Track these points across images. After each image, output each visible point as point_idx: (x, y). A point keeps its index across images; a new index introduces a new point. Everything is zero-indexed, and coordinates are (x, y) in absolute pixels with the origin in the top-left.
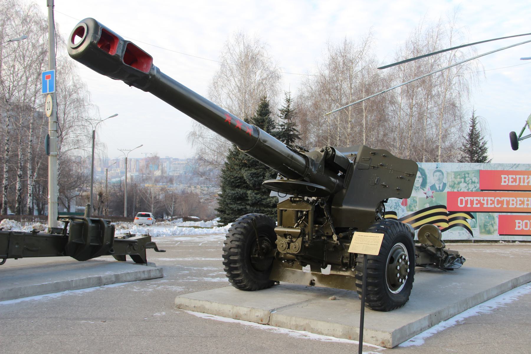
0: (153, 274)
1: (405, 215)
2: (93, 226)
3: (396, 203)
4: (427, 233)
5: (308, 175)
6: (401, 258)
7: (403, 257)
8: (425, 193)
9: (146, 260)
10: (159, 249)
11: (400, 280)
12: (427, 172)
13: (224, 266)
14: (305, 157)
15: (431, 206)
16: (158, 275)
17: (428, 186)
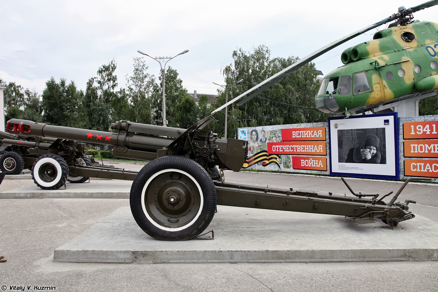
12: (258, 132)
17: (259, 140)
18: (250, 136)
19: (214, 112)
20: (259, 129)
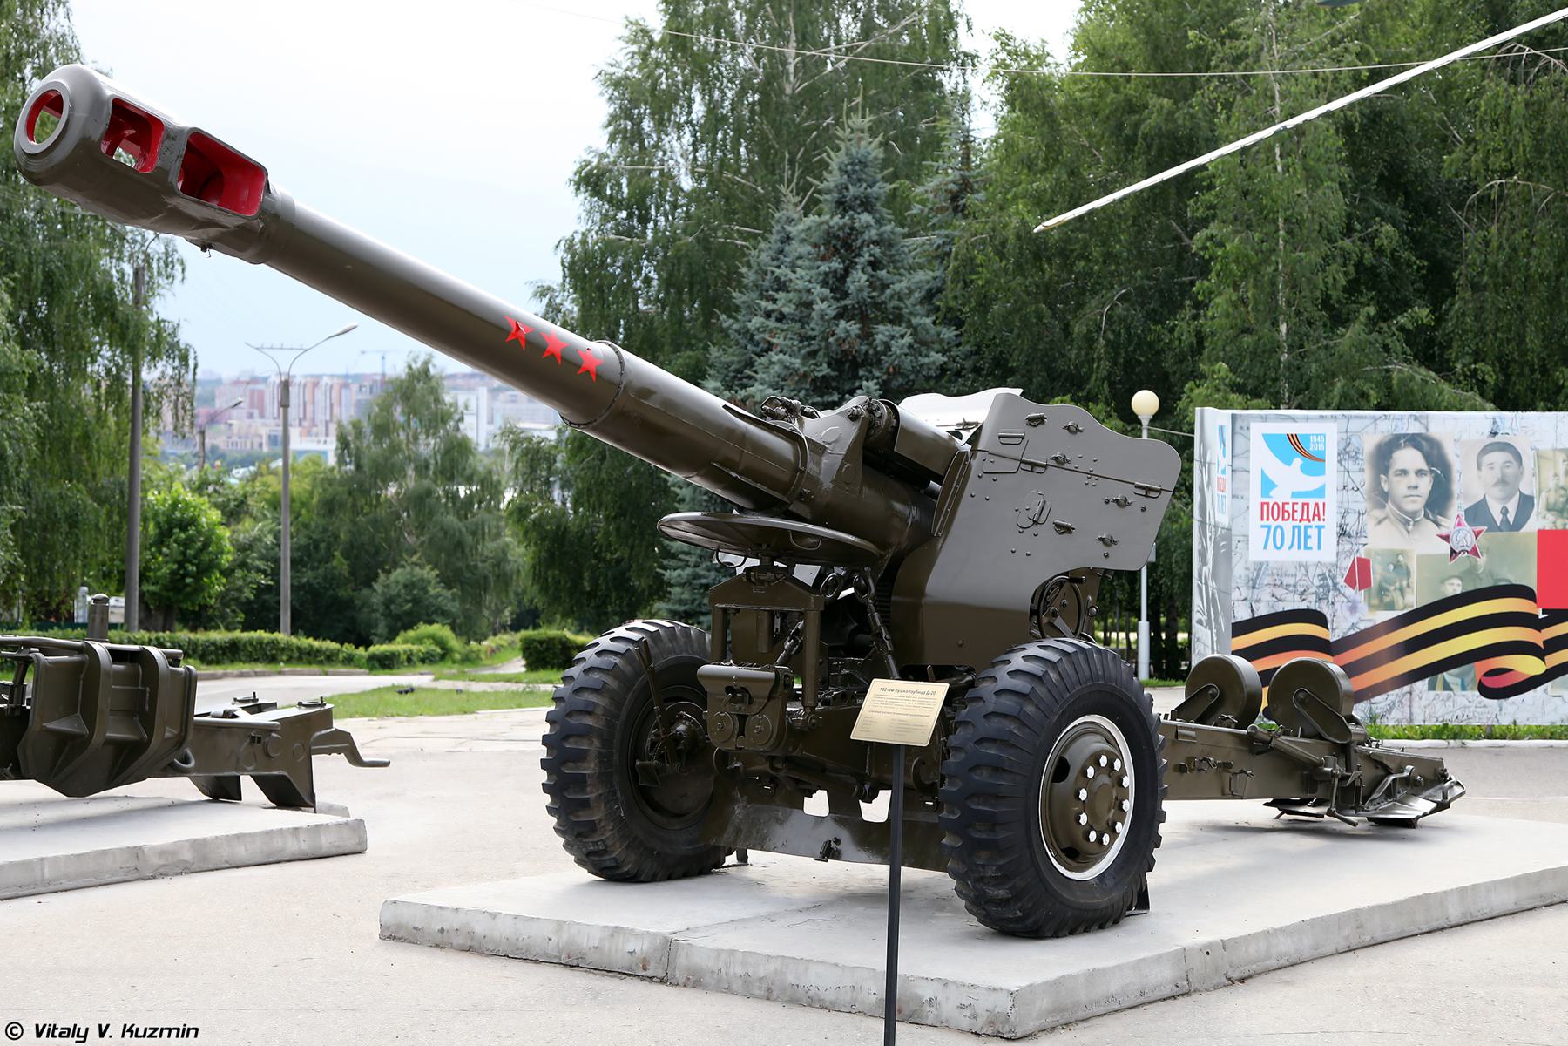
0: (326, 842)
1: (1363, 626)
2: (116, 672)
3: (1323, 577)
4: (1303, 691)
5: (802, 494)
6: (1097, 764)
7: (1104, 761)
8: (1446, 538)
9: (312, 796)
10: (366, 754)
11: (1093, 836)
12: (1451, 452)
13: (547, 799)
14: (793, 437)
15: (1471, 588)
16: (351, 844)
17: (1457, 508)
18: (1364, 478)
19: (1040, 227)
20: (1462, 429)
